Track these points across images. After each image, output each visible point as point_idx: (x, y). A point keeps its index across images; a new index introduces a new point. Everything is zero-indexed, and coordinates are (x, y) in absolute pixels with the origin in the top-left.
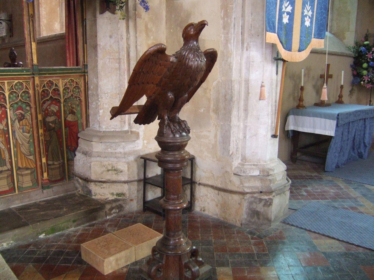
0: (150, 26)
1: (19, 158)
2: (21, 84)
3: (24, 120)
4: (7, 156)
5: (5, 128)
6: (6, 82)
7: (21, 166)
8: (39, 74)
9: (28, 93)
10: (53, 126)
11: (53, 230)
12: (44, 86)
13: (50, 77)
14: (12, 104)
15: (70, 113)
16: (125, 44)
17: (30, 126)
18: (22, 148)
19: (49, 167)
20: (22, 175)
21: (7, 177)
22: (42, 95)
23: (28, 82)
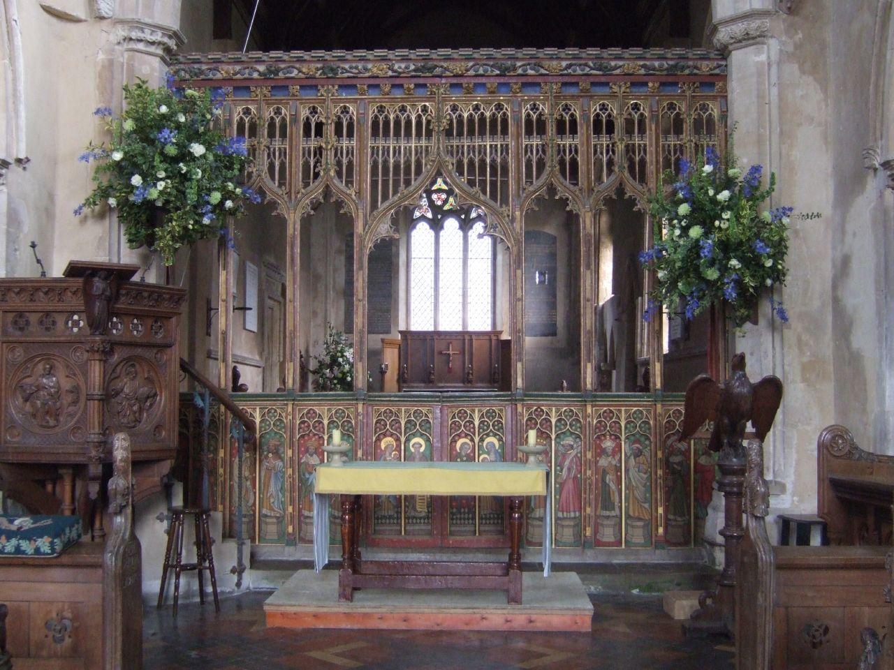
0: (805, 337)
1: (631, 505)
2: (641, 412)
6: (623, 409)
8: (662, 401)
9: (649, 423)
10: (679, 468)
11: (650, 588)
12: (669, 416)
13: (677, 405)
15: (703, 454)
16: (771, 362)
19: (669, 522)
22: (666, 428)
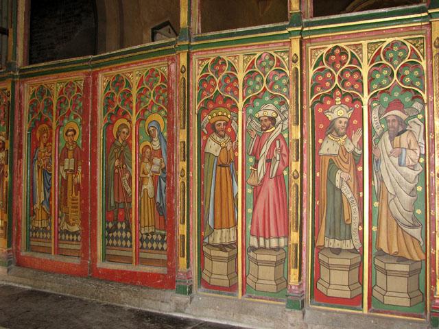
3: (404, 136)
4: (356, 215)
5: (356, 150)
6: (365, 43)
7: (386, 250)
14: (375, 94)
17: (418, 152)
18: (392, 205)
20: (386, 272)
21: (351, 267)
23: (360, 47)
